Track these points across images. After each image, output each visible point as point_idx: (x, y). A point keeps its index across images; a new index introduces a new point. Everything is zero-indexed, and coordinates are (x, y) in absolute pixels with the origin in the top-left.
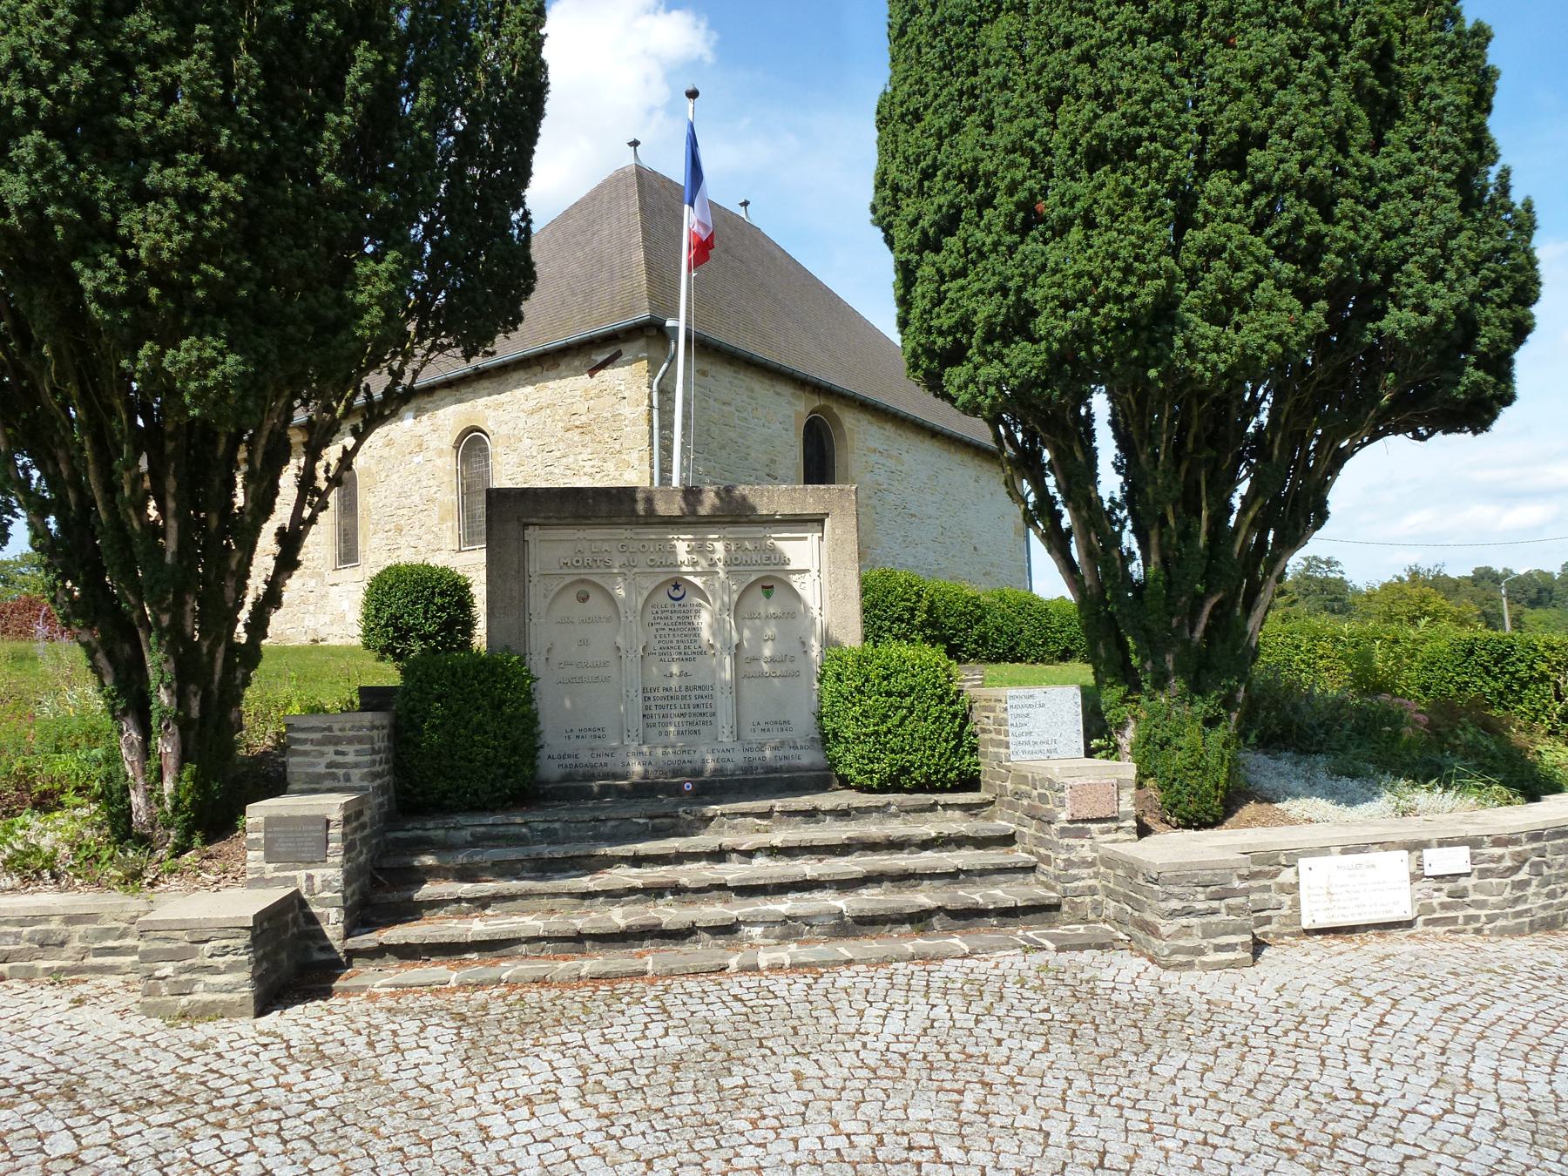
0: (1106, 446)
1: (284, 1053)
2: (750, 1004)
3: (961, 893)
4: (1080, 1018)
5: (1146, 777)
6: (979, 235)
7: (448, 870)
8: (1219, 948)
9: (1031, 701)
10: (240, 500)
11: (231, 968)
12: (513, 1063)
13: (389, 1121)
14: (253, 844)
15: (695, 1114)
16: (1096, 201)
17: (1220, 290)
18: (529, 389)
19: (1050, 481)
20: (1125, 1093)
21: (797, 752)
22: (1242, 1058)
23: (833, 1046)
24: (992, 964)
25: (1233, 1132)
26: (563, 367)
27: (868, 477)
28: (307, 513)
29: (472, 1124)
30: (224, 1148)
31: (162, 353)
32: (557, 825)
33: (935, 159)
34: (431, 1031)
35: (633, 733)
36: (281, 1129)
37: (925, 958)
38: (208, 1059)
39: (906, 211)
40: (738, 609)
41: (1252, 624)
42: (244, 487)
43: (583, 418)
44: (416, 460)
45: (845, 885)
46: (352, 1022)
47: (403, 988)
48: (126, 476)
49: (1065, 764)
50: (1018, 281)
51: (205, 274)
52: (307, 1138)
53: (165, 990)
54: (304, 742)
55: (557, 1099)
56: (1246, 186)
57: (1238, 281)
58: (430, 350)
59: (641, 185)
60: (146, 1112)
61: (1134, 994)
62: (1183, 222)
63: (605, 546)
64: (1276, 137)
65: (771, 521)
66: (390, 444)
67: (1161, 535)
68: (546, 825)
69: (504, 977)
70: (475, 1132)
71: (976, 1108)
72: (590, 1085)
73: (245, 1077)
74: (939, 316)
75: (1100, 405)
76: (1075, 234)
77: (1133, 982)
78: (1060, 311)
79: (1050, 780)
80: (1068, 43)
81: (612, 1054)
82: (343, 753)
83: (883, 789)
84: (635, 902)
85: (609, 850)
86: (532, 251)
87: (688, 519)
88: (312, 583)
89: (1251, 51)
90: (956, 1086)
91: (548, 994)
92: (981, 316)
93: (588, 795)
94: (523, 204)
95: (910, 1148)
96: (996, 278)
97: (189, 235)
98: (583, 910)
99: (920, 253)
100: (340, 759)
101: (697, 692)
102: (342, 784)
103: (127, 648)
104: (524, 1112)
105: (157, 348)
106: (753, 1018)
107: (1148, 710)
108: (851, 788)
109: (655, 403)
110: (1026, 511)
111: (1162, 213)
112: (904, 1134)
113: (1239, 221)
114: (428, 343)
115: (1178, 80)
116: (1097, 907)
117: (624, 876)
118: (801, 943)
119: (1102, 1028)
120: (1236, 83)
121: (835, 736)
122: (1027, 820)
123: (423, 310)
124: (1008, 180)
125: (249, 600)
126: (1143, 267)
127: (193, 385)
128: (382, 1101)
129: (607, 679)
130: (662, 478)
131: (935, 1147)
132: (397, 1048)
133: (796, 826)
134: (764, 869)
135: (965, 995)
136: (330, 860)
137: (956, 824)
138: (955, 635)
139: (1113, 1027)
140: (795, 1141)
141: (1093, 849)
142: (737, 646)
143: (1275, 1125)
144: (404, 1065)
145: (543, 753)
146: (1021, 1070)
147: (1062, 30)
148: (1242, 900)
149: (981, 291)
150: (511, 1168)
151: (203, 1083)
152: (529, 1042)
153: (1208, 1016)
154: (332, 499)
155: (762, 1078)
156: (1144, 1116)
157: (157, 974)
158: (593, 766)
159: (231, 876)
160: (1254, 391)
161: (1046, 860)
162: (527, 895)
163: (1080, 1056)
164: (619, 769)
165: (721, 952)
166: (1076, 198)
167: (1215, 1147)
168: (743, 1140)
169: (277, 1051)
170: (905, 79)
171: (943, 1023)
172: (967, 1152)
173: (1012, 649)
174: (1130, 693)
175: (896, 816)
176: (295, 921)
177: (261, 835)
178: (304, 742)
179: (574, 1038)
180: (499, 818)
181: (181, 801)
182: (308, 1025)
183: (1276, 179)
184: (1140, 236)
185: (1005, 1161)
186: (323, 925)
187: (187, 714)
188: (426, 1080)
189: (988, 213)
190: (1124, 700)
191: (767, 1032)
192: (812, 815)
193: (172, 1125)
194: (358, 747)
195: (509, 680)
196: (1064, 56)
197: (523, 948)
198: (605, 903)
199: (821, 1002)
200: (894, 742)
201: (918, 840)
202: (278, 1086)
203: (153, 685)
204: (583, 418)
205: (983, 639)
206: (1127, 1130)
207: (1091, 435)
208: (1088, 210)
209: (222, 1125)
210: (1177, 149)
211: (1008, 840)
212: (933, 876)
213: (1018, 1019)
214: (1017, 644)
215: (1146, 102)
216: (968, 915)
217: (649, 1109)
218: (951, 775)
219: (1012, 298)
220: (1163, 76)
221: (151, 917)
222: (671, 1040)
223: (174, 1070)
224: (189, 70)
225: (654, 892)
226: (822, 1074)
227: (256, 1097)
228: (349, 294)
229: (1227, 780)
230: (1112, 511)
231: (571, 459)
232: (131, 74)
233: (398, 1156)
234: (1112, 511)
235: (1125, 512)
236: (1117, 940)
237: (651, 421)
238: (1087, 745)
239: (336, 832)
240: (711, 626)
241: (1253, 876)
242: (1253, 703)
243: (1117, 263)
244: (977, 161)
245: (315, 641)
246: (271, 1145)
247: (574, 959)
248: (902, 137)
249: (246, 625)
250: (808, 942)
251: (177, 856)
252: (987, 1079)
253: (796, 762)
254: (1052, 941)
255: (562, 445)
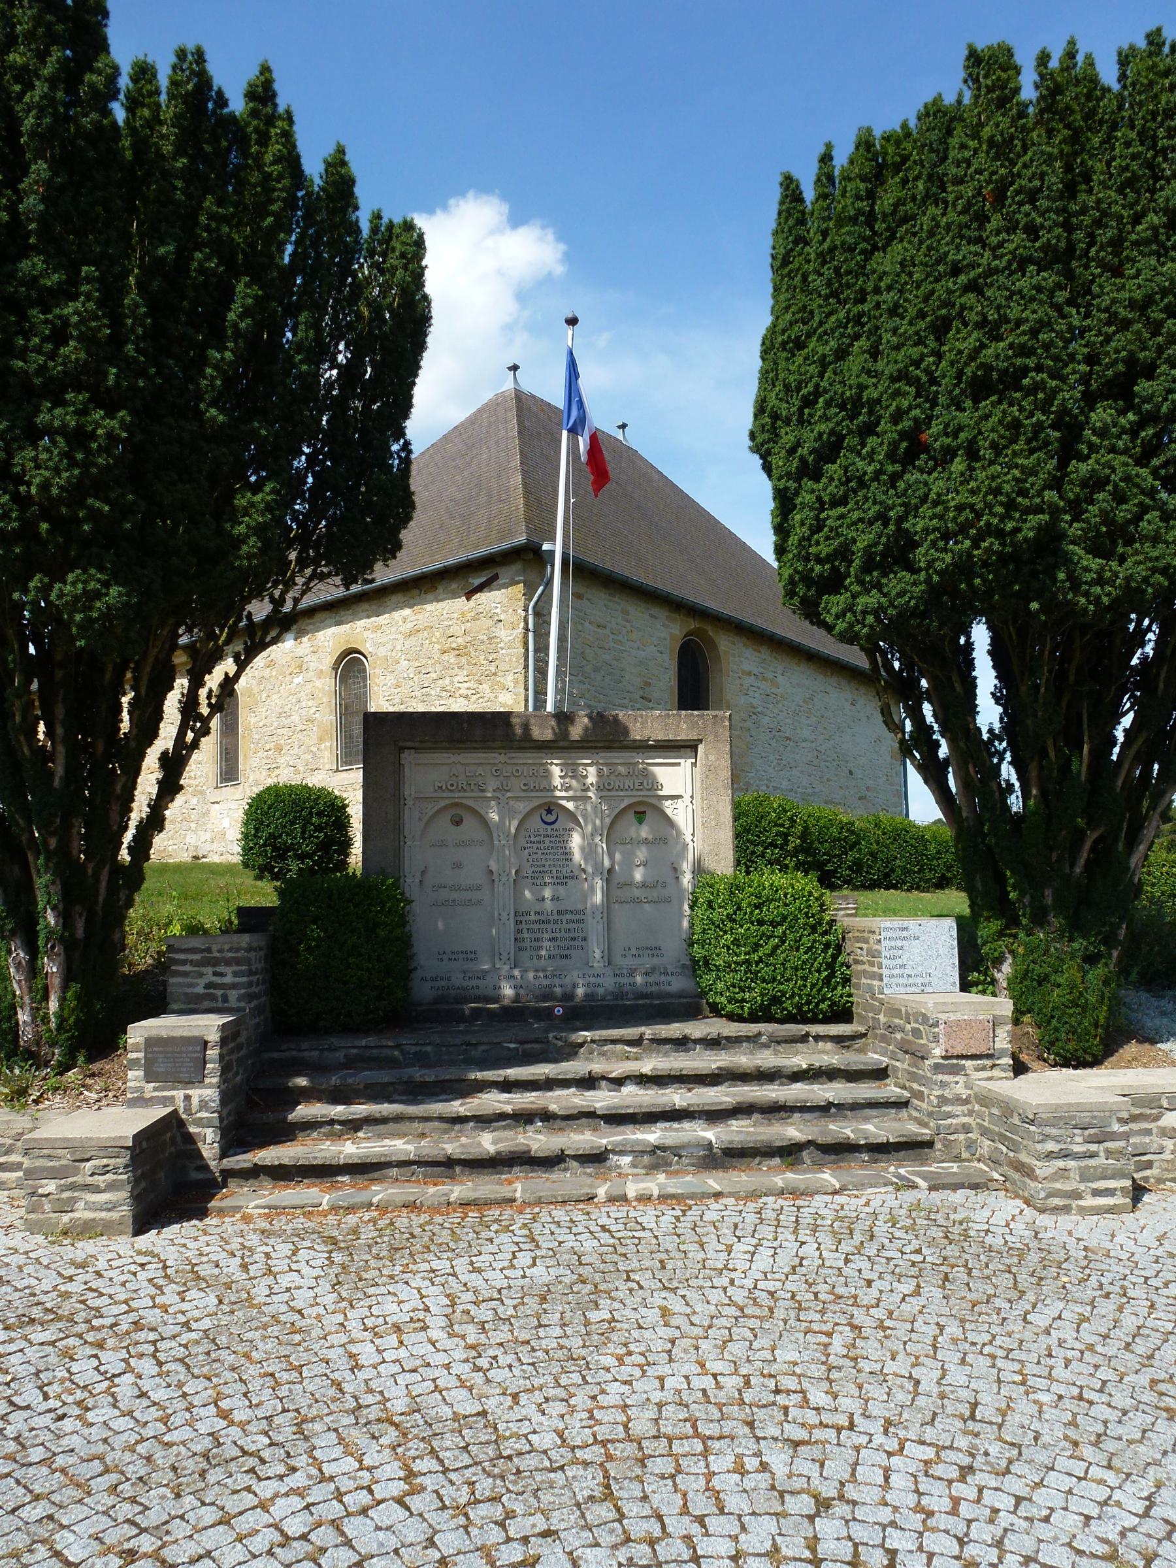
0: (986, 676)
1: (160, 1273)
2: (618, 1235)
3: (832, 1127)
4: (952, 1261)
5: (1023, 1013)
6: (860, 464)
7: (322, 1091)
8: (1096, 1193)
9: (905, 934)
10: (125, 726)
11: (111, 1187)
12: (383, 1290)
13: (261, 1345)
14: (134, 1064)
15: (562, 1347)
16: (980, 433)
17: (1103, 523)
18: (407, 612)
19: (927, 709)
20: (998, 1342)
21: (669, 978)
22: (1120, 1309)
23: (701, 1282)
24: (863, 1201)
25: (1109, 1388)
26: (440, 590)
27: (742, 700)
28: (190, 736)
29: (341, 1350)
30: (102, 1369)
31: (50, 587)
32: (429, 1049)
33: (817, 386)
34: (303, 1255)
35: (504, 957)
36: (157, 1350)
37: (794, 1193)
38: (88, 1277)
39: (785, 439)
40: (611, 832)
41: (1133, 861)
42: (129, 713)
43: (460, 640)
44: (296, 681)
45: (714, 1116)
46: (227, 1243)
47: (276, 1210)
48: (18, 703)
49: (941, 998)
50: (900, 510)
51: (91, 509)
52: (182, 1360)
53: (47, 1207)
54: (184, 963)
55: (425, 1328)
56: (1131, 416)
57: (1123, 513)
58: (311, 579)
59: (520, 409)
60: (28, 1330)
61: (1008, 1238)
62: (1067, 453)
63: (480, 771)
64: (1164, 368)
65: (644, 747)
66: (271, 665)
67: (1041, 768)
68: (418, 1048)
69: (375, 1200)
70: (345, 1359)
71: (845, 1352)
72: (458, 1314)
73: (122, 1297)
74: (818, 543)
75: (980, 635)
76: (958, 465)
77: (1007, 1225)
78: (941, 544)
79: (924, 1015)
80: (956, 270)
81: (480, 1283)
82: (221, 975)
83: (753, 1018)
84: (504, 1128)
85: (479, 1075)
86: (411, 481)
87: (562, 744)
88: (194, 801)
89: (1140, 280)
90: (824, 1328)
91: (418, 1219)
92: (860, 545)
93: (460, 1018)
94: (403, 435)
95: (777, 1391)
96: (877, 507)
97: (76, 472)
98: (453, 1134)
99: (798, 480)
100: (218, 980)
101: (569, 917)
102: (220, 1005)
103: (16, 870)
104: (393, 1340)
105: (46, 580)
106: (620, 1250)
107: (1026, 944)
108: (721, 1016)
109: (531, 626)
110: (902, 742)
111: (1047, 443)
112: (771, 1376)
113: (1125, 452)
114: (308, 572)
115: (1067, 309)
116: (971, 1145)
117: (494, 1101)
118: (670, 1174)
119: (975, 1272)
120: (1123, 313)
121: (706, 963)
122: (900, 1054)
123: (304, 540)
124: (893, 408)
125: (133, 824)
126: (1026, 502)
127: (78, 617)
128: (254, 1324)
129: (479, 902)
130: (536, 700)
131: (802, 1392)
132: (269, 1271)
133: (666, 1055)
134: (632, 1097)
135: (834, 1233)
136: (207, 1081)
137: (828, 1056)
138: (829, 861)
139: (987, 1272)
140: (661, 1379)
141: (967, 1087)
142: (610, 871)
143: (1154, 1382)
144: (276, 1289)
145: (419, 973)
146: (891, 1313)
147: (950, 257)
148: (1122, 1144)
149: (861, 520)
150: (379, 1398)
151: (83, 1302)
152: (399, 1268)
153: (1085, 1263)
154: (215, 723)
155: (628, 1312)
156: (1017, 1367)
157: (40, 1191)
158: (465, 989)
159: (113, 1094)
160: (1139, 622)
161: (920, 1096)
162: (398, 1118)
163: (952, 1301)
164: (490, 992)
165: (589, 1181)
166: (960, 428)
167: (1091, 1403)
168: (609, 1377)
169: (153, 1271)
170: (787, 308)
171: (812, 1263)
172: (835, 1397)
173: (887, 875)
174: (1007, 927)
175: (766, 1046)
176: (173, 1141)
177: (141, 1055)
178: (184, 963)
179: (442, 1265)
180: (371, 1040)
181: (66, 1020)
182: (184, 1246)
183: (1164, 409)
184: (1023, 470)
185: (874, 1409)
186: (200, 1144)
187: (72, 935)
188: (296, 1304)
189: (872, 441)
190: (1001, 934)
191: (634, 1265)
192: (682, 1043)
193: (52, 1343)
194: (235, 968)
195: (383, 903)
196: (950, 284)
197: (394, 1172)
198: (475, 1128)
199: (689, 1235)
200: (766, 971)
201: (789, 1071)
202: (154, 1306)
203: (40, 906)
204: (460, 640)
205: (857, 866)
206: (999, 1381)
207: (970, 664)
208: (972, 442)
209: (100, 1345)
210: (1063, 379)
211: (880, 1074)
212: (803, 1109)
213: (889, 1259)
214: (893, 870)
215: (1034, 333)
216: (840, 1150)
217: (516, 1341)
218: (824, 1006)
219: (892, 527)
220: (1052, 305)
221: (36, 1135)
222: (538, 1271)
223: (55, 1288)
224: (76, 312)
225: (524, 1118)
226: (689, 1310)
227: (133, 1317)
228: (228, 526)
229: (1107, 1019)
230: (990, 742)
231: (447, 681)
232: (23, 317)
233: (269, 1381)
234: (990, 742)
235: (1004, 744)
236: (992, 1180)
237: (526, 644)
238: (963, 978)
239: (213, 1053)
240: (582, 849)
241: (1134, 1118)
242: (1135, 938)
243: (999, 498)
244: (862, 387)
245: (196, 858)
246: (147, 1366)
247: (444, 1184)
248: (782, 364)
249: (129, 848)
250: (676, 1173)
251: (61, 1074)
252: (856, 1322)
253: (667, 988)
254: (924, 1179)
255: (438, 667)
